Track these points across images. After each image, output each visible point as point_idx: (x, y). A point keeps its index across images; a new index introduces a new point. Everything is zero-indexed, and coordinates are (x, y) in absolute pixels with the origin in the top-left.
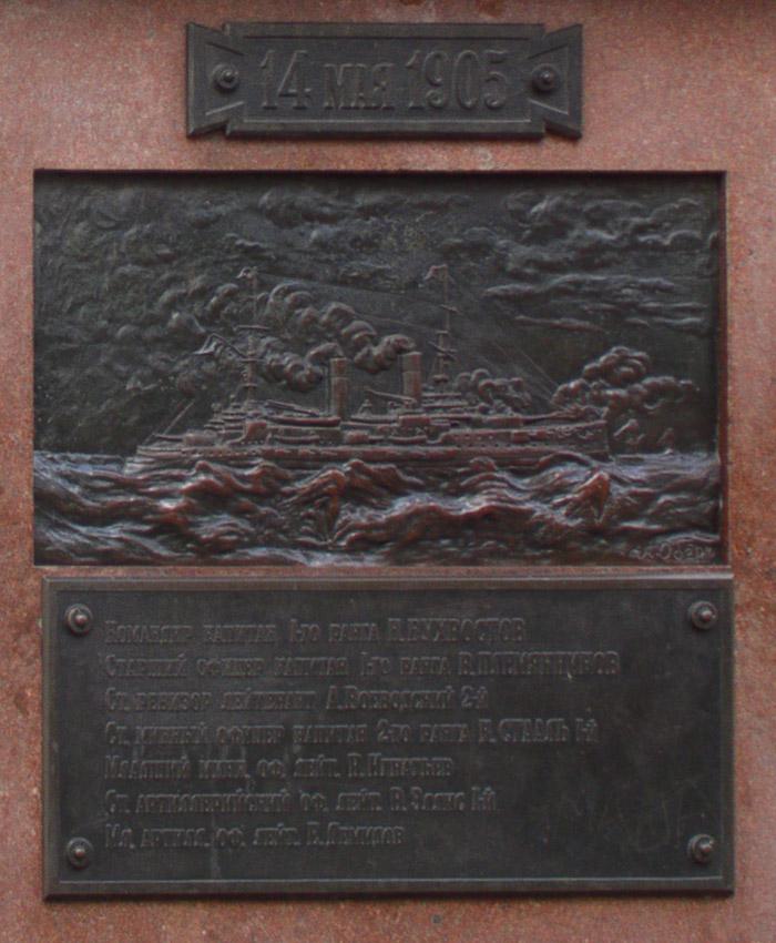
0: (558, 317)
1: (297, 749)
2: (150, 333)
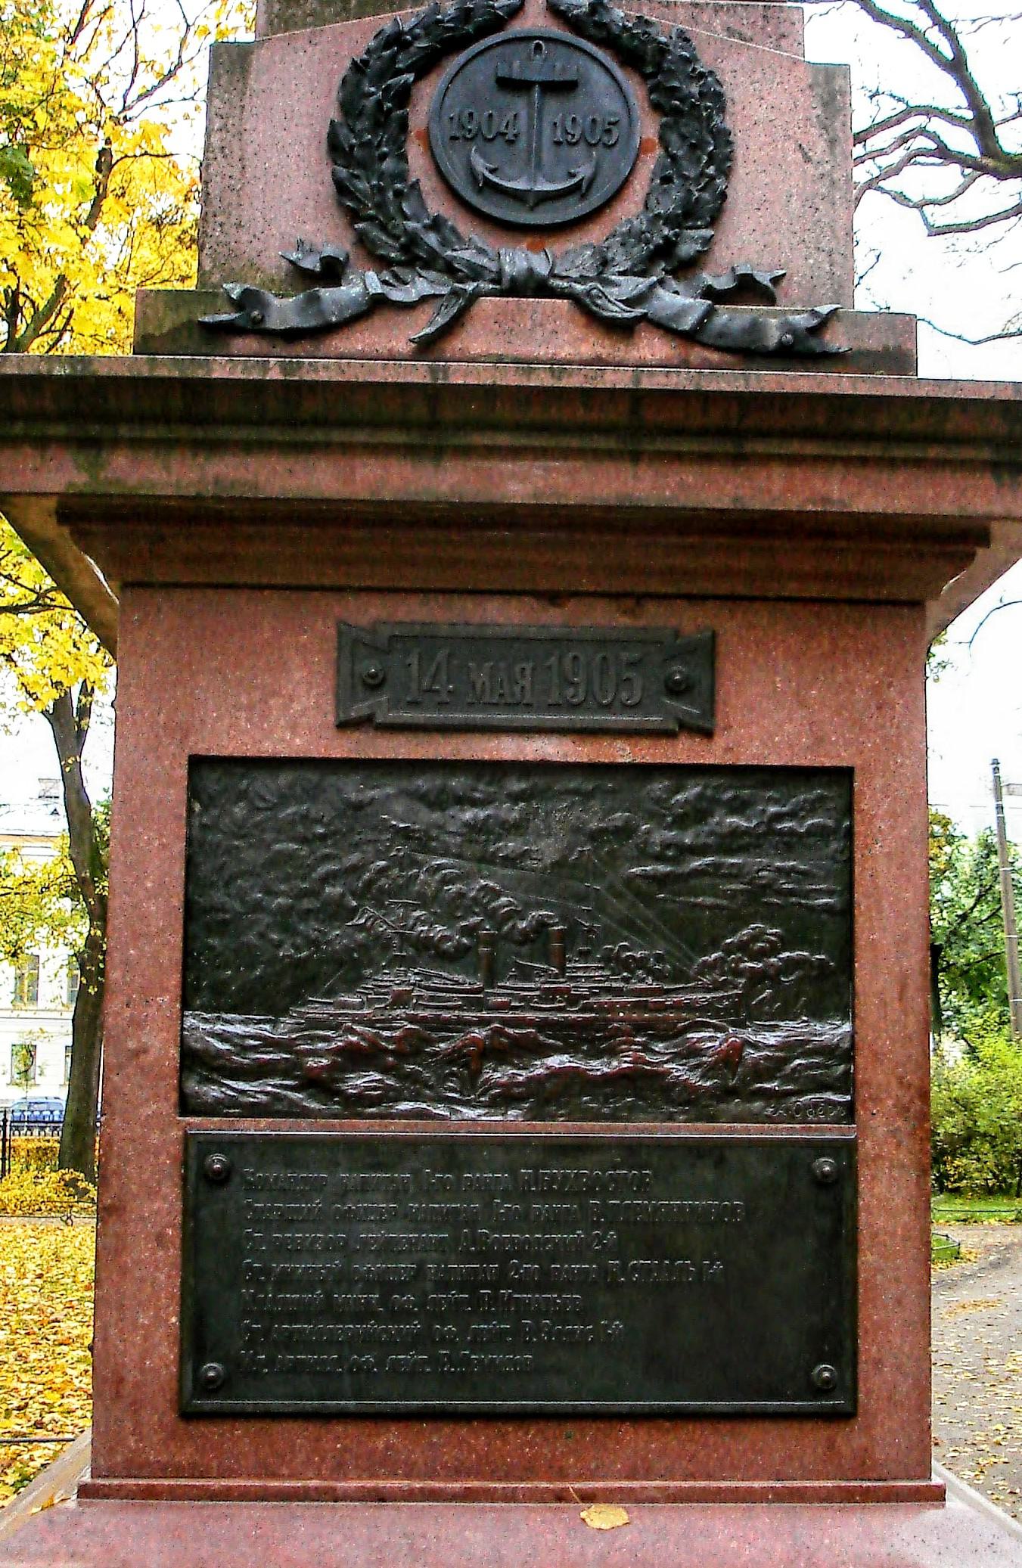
0: (697, 896)
1: (429, 1286)
2: (307, 904)
